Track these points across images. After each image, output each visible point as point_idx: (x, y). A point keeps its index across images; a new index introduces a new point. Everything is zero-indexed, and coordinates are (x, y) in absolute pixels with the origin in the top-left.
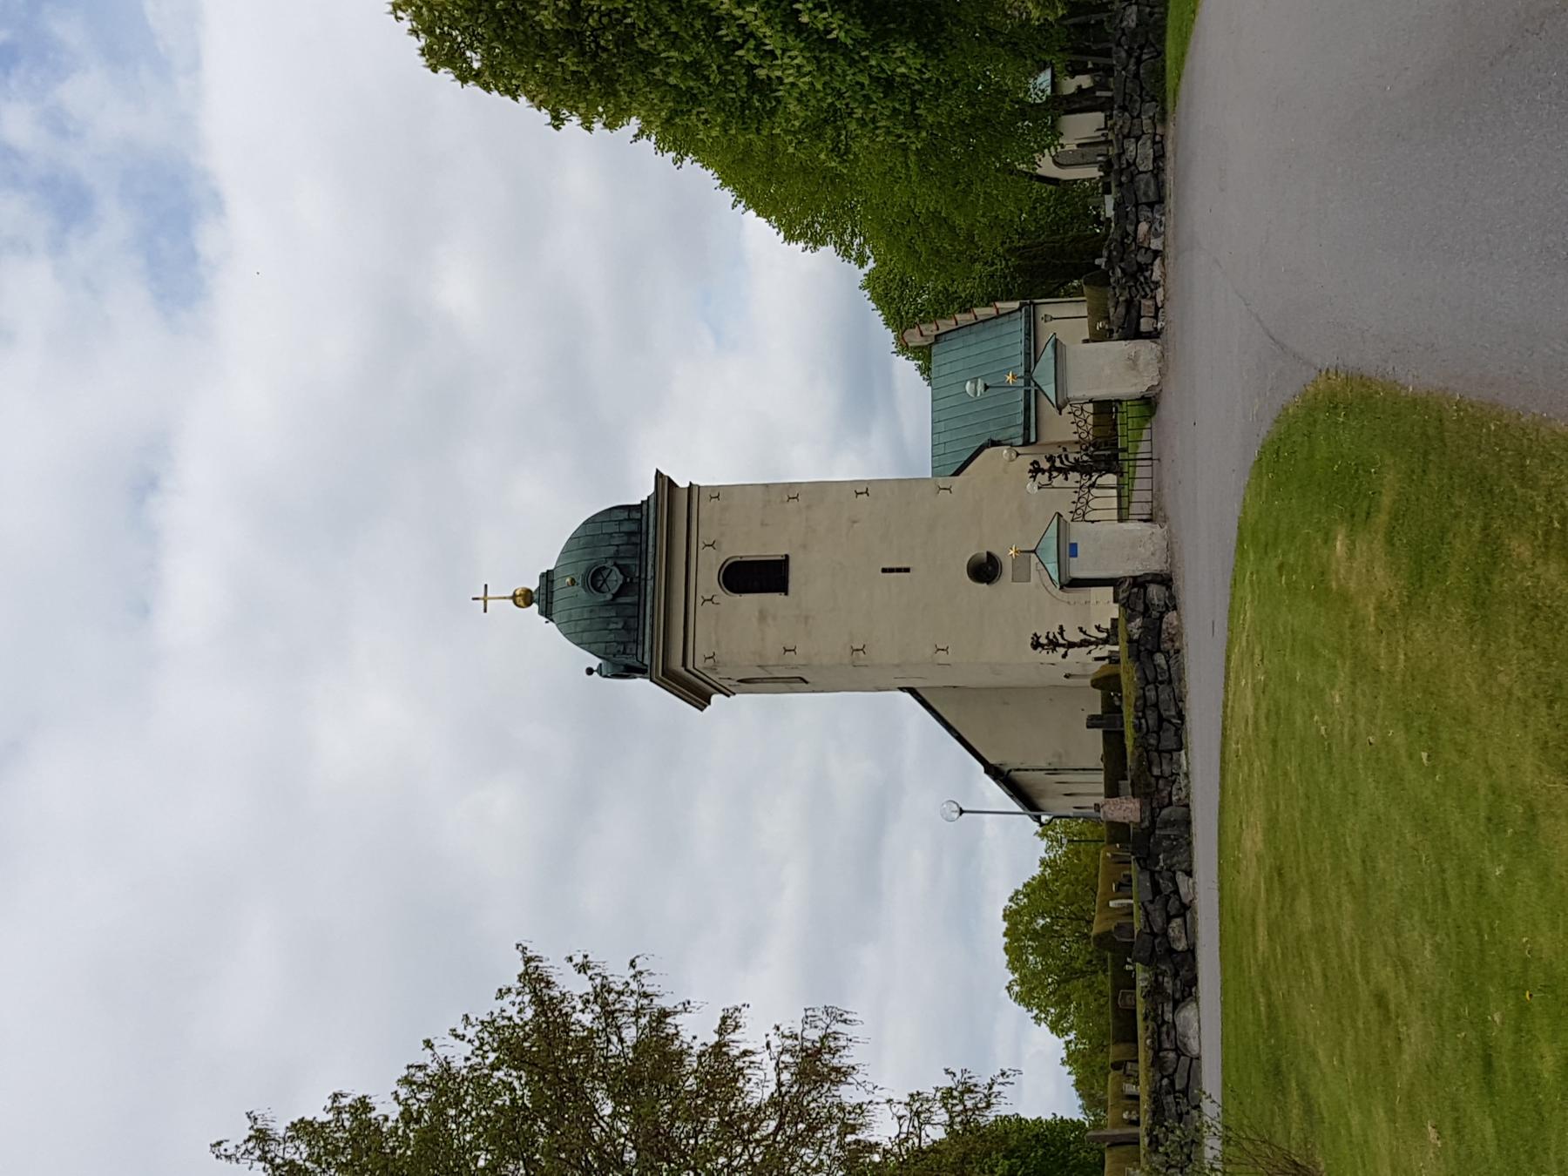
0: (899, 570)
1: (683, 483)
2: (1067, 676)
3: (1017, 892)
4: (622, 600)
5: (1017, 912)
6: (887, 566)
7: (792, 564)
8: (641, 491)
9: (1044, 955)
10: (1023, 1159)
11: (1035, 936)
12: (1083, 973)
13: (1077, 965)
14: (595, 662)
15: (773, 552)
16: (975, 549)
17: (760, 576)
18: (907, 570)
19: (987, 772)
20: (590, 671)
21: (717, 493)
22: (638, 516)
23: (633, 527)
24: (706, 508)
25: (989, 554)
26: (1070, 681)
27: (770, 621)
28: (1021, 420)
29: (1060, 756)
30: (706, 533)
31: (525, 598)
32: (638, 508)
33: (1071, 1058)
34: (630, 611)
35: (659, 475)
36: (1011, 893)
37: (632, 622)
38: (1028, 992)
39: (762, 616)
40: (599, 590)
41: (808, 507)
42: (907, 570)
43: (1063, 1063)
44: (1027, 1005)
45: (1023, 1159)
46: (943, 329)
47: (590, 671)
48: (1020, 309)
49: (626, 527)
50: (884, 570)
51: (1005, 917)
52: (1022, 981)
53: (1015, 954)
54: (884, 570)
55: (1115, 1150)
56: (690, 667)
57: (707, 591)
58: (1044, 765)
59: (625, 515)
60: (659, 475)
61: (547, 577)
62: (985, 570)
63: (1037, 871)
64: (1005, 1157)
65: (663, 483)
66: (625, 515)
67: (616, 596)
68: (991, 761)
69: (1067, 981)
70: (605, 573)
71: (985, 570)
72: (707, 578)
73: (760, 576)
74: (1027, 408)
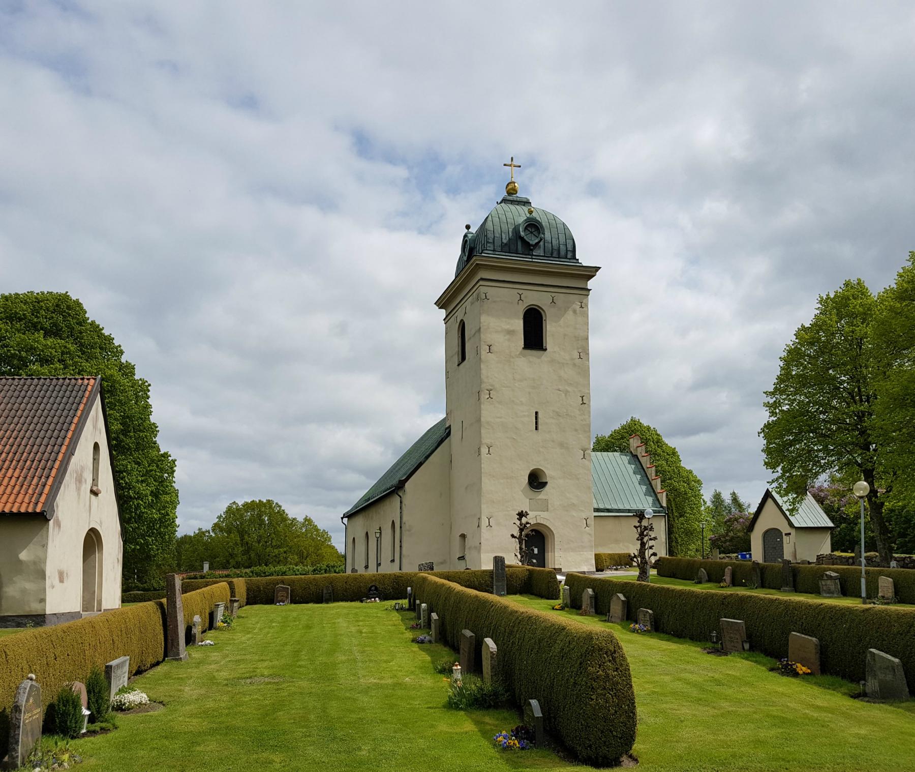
0: (536, 423)
1: (591, 284)
2: (463, 536)
3: (280, 507)
4: (519, 243)
5: (270, 507)
6: (540, 415)
7: (541, 352)
8: (584, 258)
9: (250, 520)
10: (151, 506)
11: (260, 516)
12: (242, 540)
13: (246, 537)
14: (473, 230)
15: (549, 340)
16: (550, 473)
17: (534, 335)
19: (400, 481)
20: (468, 227)
22: (569, 256)
23: (563, 253)
24: (574, 299)
25: (546, 483)
26: (457, 540)
27: (507, 337)
28: (601, 507)
29: (409, 531)
30: (561, 298)
31: (511, 190)
32: (574, 257)
33: (201, 533)
34: (513, 247)
35: (597, 269)
36: (280, 504)
37: (507, 249)
38: (232, 512)
39: (511, 332)
40: (526, 229)
41: (574, 365)
42: (536, 429)
43: (200, 529)
44: (226, 512)
45: (151, 506)
46: (643, 460)
47: (468, 227)
48: (662, 507)
49: (563, 248)
50: (537, 413)
51: (268, 501)
52: (238, 510)
53: (249, 506)
54: (537, 413)
55: (157, 618)
56: (481, 283)
57: (526, 297)
58: (404, 519)
59: (570, 247)
60: (597, 269)
62: (536, 481)
63: (290, 516)
64: (152, 492)
65: (591, 272)
66: (570, 247)
67: (522, 239)
69: (238, 532)
70: (535, 233)
71: (536, 481)
72: (534, 298)
73: (534, 335)
74: (608, 511)
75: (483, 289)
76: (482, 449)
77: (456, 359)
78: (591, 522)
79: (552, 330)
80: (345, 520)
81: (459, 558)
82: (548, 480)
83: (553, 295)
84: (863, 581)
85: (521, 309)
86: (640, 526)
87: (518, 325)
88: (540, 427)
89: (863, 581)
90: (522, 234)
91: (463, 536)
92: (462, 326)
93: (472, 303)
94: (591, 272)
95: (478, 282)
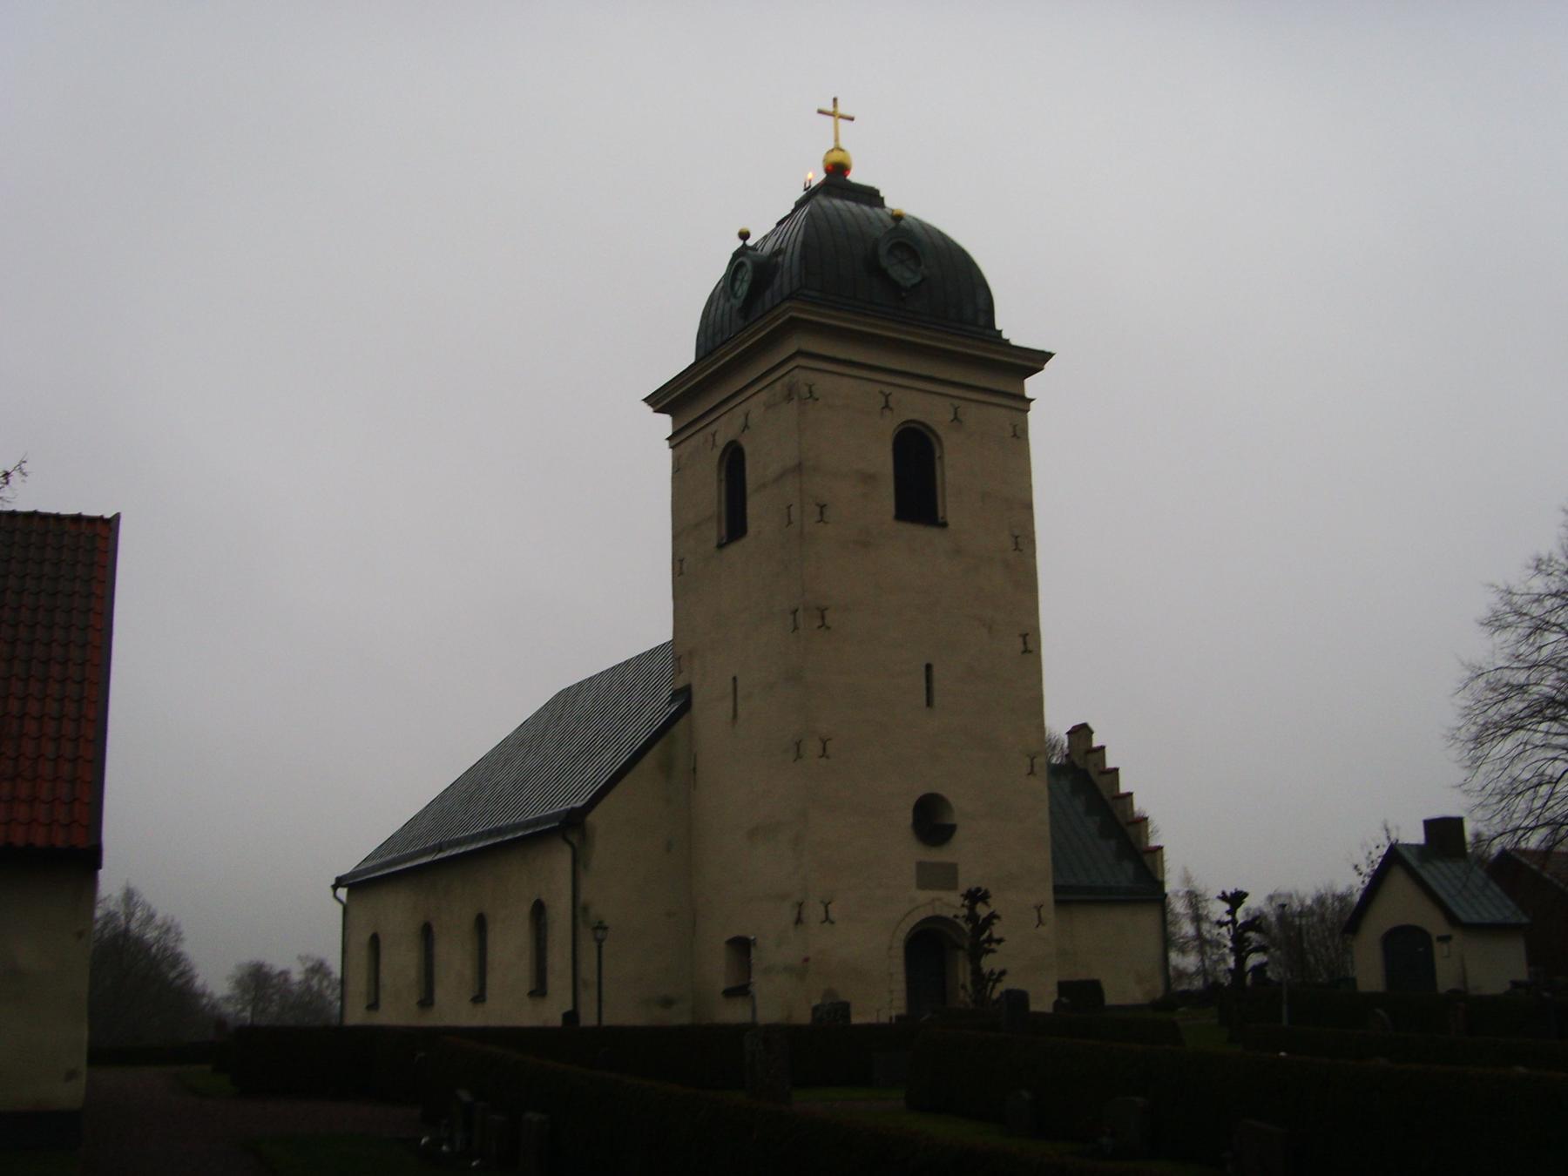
0: (929, 690)
8: (1014, 322)
15: (951, 506)
16: (962, 804)
18: (929, 703)
20: (744, 236)
21: (1020, 434)
31: (837, 171)
35: (1046, 356)
40: (890, 252)
42: (929, 703)
50: (929, 667)
60: (1046, 356)
61: (871, 196)
65: (1035, 360)
68: (591, 818)
72: (918, 406)
75: (801, 376)
76: (1522, 732)
77: (712, 533)
80: (343, 893)
81: (729, 993)
83: (957, 403)
85: (888, 427)
87: (883, 461)
88: (937, 699)
90: (884, 262)
91: (742, 946)
92: (734, 461)
93: (769, 406)
94: (1035, 360)
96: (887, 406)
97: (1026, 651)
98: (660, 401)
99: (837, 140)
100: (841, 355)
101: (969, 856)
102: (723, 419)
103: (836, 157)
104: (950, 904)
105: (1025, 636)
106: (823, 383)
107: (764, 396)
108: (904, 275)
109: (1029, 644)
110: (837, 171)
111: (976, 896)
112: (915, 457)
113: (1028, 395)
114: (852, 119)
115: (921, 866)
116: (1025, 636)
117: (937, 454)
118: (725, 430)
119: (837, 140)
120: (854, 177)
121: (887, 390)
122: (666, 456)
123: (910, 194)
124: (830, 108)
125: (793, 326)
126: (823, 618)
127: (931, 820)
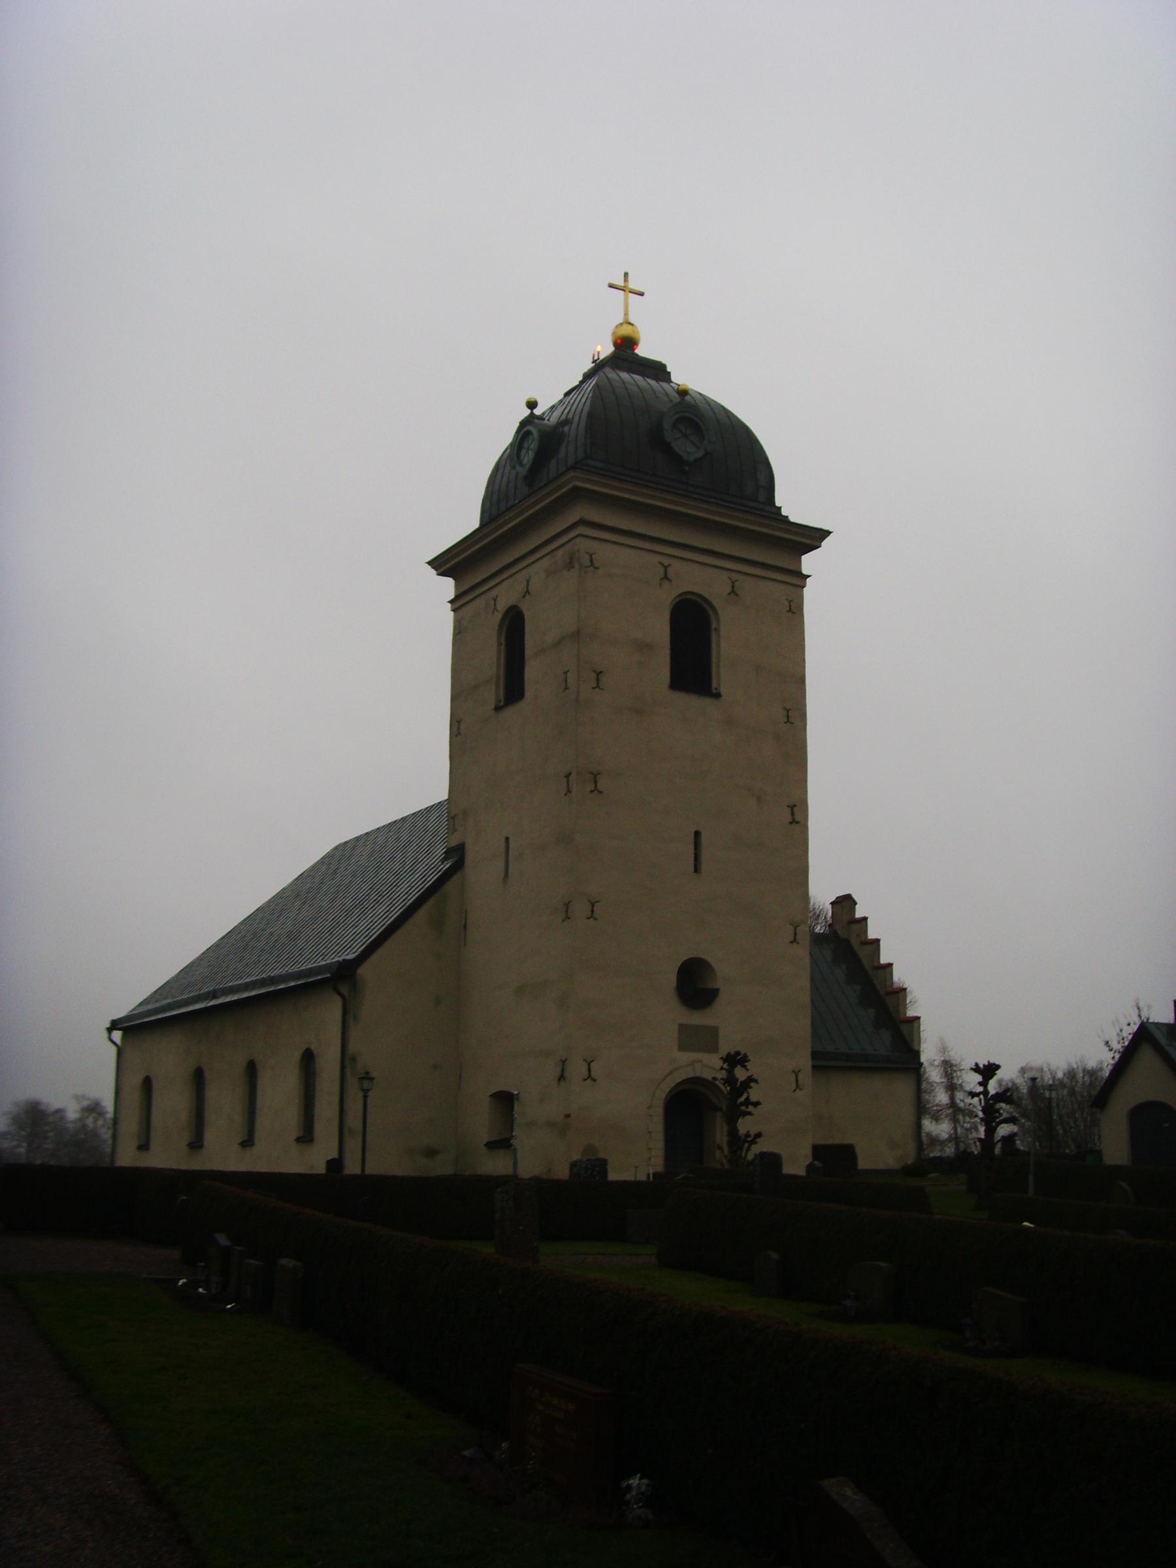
1: (808, 563)
8: (795, 501)
15: (724, 677)
18: (697, 869)
21: (795, 609)
31: (625, 345)
35: (824, 534)
40: (675, 425)
42: (697, 869)
47: (532, 405)
50: (697, 834)
56: (581, 530)
60: (824, 534)
61: (658, 371)
65: (813, 537)
68: (364, 971)
72: (703, 580)
75: (583, 545)
78: (806, 1077)
79: (731, 641)
81: (491, 1145)
82: (719, 984)
83: (734, 576)
84: (1031, 1178)
85: (667, 597)
86: (986, 1092)
87: (659, 630)
88: (704, 867)
89: (1031, 1178)
90: (669, 436)
94: (813, 537)
95: (575, 537)
96: (666, 577)
97: (794, 822)
98: (443, 564)
99: (626, 314)
100: (495, 569)
101: (730, 1021)
102: (506, 583)
103: (626, 331)
104: (710, 1066)
105: (792, 807)
106: (605, 553)
107: (545, 563)
108: (688, 449)
109: (796, 815)
110: (625, 345)
111: (735, 1060)
112: (692, 627)
113: (805, 571)
114: (642, 294)
115: (683, 1028)
116: (792, 807)
117: (714, 626)
118: (506, 595)
119: (626, 314)
120: (642, 351)
121: (666, 561)
122: (447, 618)
123: (699, 370)
124: (621, 283)
125: (576, 495)
126: (596, 782)
127: (695, 985)
